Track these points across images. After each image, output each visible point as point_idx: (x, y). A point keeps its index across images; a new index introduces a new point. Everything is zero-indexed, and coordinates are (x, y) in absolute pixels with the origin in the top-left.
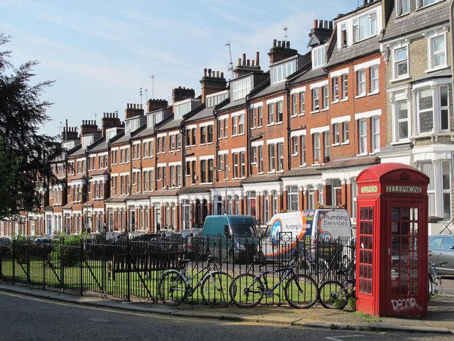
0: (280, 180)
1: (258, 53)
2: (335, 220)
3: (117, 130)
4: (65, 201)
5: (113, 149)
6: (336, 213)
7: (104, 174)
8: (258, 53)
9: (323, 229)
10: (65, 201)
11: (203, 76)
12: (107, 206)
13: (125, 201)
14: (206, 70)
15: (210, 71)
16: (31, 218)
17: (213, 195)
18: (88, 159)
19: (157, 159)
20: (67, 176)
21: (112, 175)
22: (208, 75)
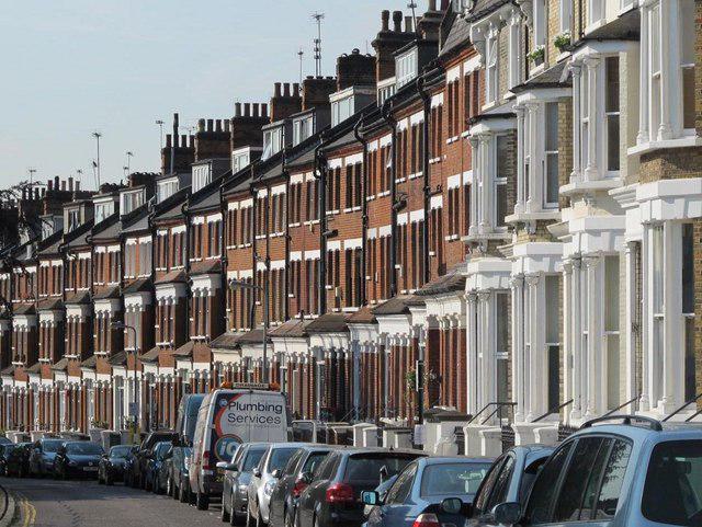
0: (406, 312)
1: (176, 116)
2: (254, 413)
3: (356, 95)
4: (149, 342)
5: (232, 206)
6: (255, 399)
7: (209, 272)
8: (176, 116)
9: (225, 428)
10: (149, 342)
11: (380, 28)
12: (217, 358)
13: (306, 336)
14: (386, 15)
15: (398, 16)
16: (120, 380)
17: (146, 372)
18: (191, 227)
19: (288, 239)
20: (154, 272)
21: (231, 275)
22: (392, 26)
